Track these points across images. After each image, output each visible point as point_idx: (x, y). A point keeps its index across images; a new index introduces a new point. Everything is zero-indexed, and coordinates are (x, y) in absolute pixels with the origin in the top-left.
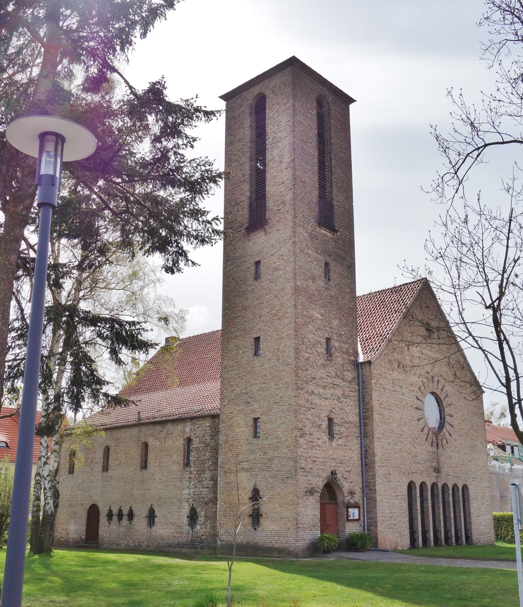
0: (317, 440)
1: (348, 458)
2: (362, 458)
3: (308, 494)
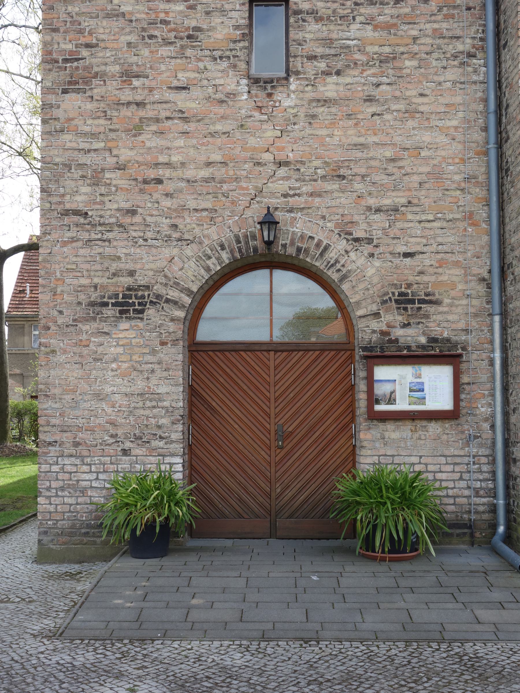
0: (171, 96)
1: (389, 154)
2: (163, 622)
3: (109, 312)
